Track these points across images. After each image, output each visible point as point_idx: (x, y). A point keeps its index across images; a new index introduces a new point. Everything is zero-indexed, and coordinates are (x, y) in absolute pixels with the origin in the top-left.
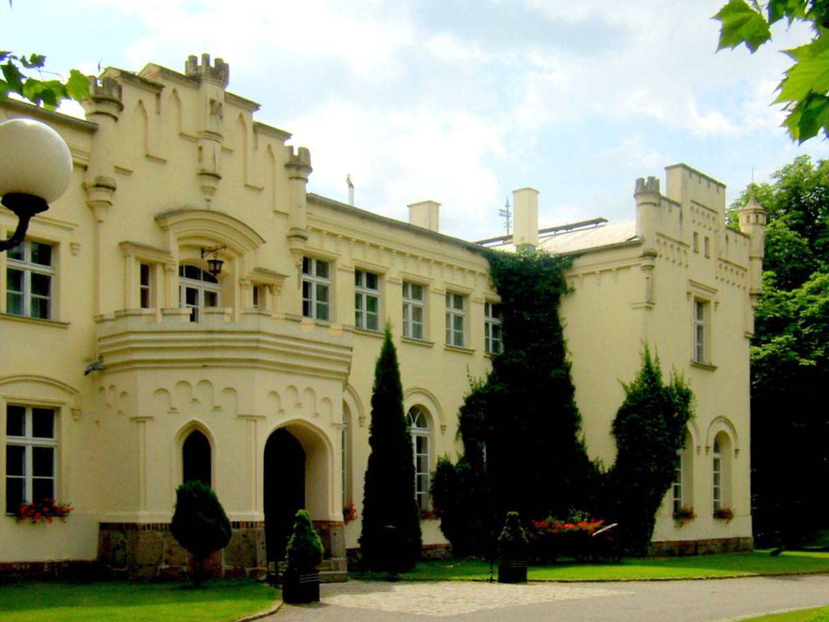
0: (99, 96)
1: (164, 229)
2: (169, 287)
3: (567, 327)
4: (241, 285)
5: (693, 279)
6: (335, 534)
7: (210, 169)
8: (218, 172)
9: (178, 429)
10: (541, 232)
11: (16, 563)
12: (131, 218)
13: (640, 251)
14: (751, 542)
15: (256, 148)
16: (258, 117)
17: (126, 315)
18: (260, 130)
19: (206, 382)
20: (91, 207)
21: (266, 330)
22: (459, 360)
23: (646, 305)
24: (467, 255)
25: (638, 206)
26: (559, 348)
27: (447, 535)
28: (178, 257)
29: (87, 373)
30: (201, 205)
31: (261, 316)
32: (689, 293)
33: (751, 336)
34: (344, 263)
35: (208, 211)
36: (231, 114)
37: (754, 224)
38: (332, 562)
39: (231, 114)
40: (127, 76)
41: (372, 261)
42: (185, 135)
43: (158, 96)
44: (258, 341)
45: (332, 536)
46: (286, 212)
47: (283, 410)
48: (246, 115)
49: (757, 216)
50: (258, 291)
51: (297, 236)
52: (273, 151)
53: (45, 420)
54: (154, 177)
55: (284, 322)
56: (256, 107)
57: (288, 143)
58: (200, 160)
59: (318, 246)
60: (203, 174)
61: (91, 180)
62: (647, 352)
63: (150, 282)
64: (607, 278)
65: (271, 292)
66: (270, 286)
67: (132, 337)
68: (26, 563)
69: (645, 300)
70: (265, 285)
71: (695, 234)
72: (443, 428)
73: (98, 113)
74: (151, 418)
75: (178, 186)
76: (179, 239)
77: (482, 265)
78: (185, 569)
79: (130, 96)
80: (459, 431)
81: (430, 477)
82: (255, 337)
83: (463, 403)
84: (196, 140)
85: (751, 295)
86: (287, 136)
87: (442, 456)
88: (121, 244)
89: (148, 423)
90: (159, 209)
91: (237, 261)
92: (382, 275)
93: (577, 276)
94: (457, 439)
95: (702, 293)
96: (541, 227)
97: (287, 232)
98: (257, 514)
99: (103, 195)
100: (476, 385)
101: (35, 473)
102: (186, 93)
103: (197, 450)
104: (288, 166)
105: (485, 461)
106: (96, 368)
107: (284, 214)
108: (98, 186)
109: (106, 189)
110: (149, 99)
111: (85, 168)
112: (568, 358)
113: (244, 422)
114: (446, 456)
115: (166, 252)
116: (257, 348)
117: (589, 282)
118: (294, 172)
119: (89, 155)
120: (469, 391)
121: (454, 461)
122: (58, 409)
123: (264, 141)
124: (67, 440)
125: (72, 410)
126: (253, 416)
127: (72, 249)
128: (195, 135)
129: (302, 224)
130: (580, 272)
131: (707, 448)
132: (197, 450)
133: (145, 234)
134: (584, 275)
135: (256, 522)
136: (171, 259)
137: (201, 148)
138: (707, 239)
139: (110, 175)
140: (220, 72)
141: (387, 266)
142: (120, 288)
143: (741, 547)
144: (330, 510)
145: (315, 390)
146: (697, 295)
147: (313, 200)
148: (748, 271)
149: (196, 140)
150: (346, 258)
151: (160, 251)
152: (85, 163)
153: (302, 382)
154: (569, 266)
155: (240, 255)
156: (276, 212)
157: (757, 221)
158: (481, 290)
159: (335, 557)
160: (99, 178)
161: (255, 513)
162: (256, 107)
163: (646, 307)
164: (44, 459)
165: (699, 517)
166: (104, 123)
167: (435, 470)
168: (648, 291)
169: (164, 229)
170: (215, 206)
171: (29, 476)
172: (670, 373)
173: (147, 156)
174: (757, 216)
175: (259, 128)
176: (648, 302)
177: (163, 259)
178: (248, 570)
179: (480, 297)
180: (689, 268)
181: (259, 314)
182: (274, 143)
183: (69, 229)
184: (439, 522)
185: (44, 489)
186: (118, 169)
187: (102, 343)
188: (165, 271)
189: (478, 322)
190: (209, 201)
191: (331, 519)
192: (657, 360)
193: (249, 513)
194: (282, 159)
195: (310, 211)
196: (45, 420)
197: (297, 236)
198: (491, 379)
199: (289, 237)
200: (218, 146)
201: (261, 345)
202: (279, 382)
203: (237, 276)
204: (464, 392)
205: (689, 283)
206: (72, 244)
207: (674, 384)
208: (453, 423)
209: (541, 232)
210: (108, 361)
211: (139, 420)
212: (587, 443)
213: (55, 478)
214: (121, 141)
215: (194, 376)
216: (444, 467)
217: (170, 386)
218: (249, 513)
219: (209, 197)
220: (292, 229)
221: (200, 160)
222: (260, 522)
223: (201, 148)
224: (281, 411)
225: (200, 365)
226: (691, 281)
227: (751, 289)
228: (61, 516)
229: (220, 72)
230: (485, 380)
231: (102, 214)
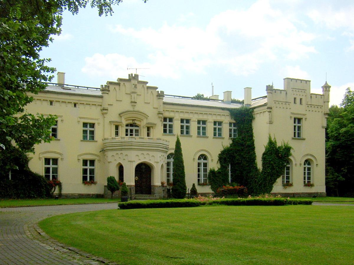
0: (103, 89)
1: (121, 117)
2: (122, 131)
3: (32, 159)
4: (143, 128)
5: (292, 112)
7: (133, 101)
9: (116, 164)
10: (252, 100)
11: (84, 194)
12: (113, 115)
13: (266, 107)
14: (325, 195)
15: (148, 93)
16: (148, 85)
18: (148, 88)
19: (121, 153)
20: (103, 114)
22: (218, 142)
23: (269, 123)
24: (221, 111)
25: (267, 93)
26: (251, 136)
27: (213, 190)
28: (125, 123)
29: (100, 152)
30: (132, 110)
32: (291, 117)
33: (326, 127)
34: (176, 119)
35: (134, 111)
36: (139, 86)
37: (325, 91)
38: (154, 195)
39: (139, 86)
40: (111, 83)
41: (186, 116)
43: (120, 85)
44: (132, 144)
45: (155, 189)
48: (144, 85)
49: (326, 88)
50: (148, 129)
51: (160, 113)
52: (153, 93)
53: (92, 162)
54: (119, 105)
55: (139, 139)
56: (147, 83)
57: (157, 90)
58: (131, 99)
59: (167, 115)
60: (132, 102)
61: (102, 108)
62: (270, 136)
63: (119, 129)
64: (262, 114)
65: (152, 128)
66: (152, 127)
67: (107, 144)
68: (86, 194)
69: (268, 121)
70: (151, 127)
71: (295, 99)
72: (212, 160)
73: (103, 93)
74: (111, 162)
75: (126, 106)
76: (125, 119)
77: (228, 113)
78: (117, 196)
79: (112, 87)
80: (218, 160)
81: (208, 174)
83: (220, 153)
84: (130, 94)
85: (324, 114)
86: (157, 88)
87: (212, 168)
88: (110, 122)
89: (111, 163)
90: (120, 112)
91: (142, 122)
92: (191, 120)
93: (255, 114)
94: (217, 163)
95: (296, 116)
96: (252, 99)
97: (157, 112)
98: (133, 183)
99: (105, 112)
100: (225, 147)
101: (49, 175)
102: (127, 84)
103: (121, 169)
104: (157, 96)
106: (103, 151)
108: (103, 109)
110: (117, 87)
111: (101, 105)
112: (254, 138)
113: (129, 162)
114: (213, 168)
115: (121, 122)
117: (258, 115)
118: (159, 97)
119: (102, 103)
120: (223, 149)
121: (216, 169)
122: (95, 160)
123: (150, 91)
124: (97, 167)
125: (98, 160)
127: (98, 124)
128: (130, 93)
129: (161, 110)
130: (256, 113)
131: (301, 164)
132: (121, 169)
133: (116, 118)
134: (257, 114)
137: (131, 96)
138: (301, 99)
139: (106, 106)
140: (136, 76)
141: (192, 117)
142: (110, 132)
143: (319, 196)
144: (154, 183)
145: (150, 154)
146: (294, 117)
147: (165, 103)
148: (323, 107)
149: (130, 94)
150: (177, 117)
151: (120, 122)
152: (101, 104)
153: (145, 152)
154: (253, 111)
155: (143, 120)
156: (154, 108)
157: (326, 90)
158: (227, 120)
160: (103, 108)
161: (132, 183)
162: (147, 83)
163: (269, 123)
164: (92, 172)
165: (294, 186)
166: (105, 96)
167: (209, 172)
168: (269, 118)
169: (121, 117)
171: (88, 175)
172: (282, 142)
173: (117, 100)
174: (326, 88)
175: (149, 88)
176: (270, 122)
177: (120, 124)
179: (227, 122)
180: (287, 109)
182: (153, 91)
184: (210, 186)
185: (92, 178)
186: (109, 105)
187: (105, 145)
188: (122, 127)
189: (226, 129)
190: (134, 108)
191: (155, 185)
192: (275, 138)
194: (155, 94)
195: (164, 106)
196: (92, 162)
197: (160, 113)
198: (231, 145)
199: (158, 114)
200: (136, 95)
202: (139, 153)
203: (142, 126)
204: (221, 150)
205: (291, 114)
206: (98, 123)
207: (283, 145)
208: (216, 158)
209: (252, 100)
210: (105, 149)
211: (109, 162)
212: (257, 163)
214: (109, 99)
215: (119, 152)
217: (115, 155)
219: (134, 107)
220: (158, 112)
221: (131, 99)
222: (133, 185)
223: (131, 96)
225: (120, 150)
226: (291, 113)
227: (324, 112)
228: (95, 184)
229: (136, 76)
230: (229, 146)
231: (105, 116)
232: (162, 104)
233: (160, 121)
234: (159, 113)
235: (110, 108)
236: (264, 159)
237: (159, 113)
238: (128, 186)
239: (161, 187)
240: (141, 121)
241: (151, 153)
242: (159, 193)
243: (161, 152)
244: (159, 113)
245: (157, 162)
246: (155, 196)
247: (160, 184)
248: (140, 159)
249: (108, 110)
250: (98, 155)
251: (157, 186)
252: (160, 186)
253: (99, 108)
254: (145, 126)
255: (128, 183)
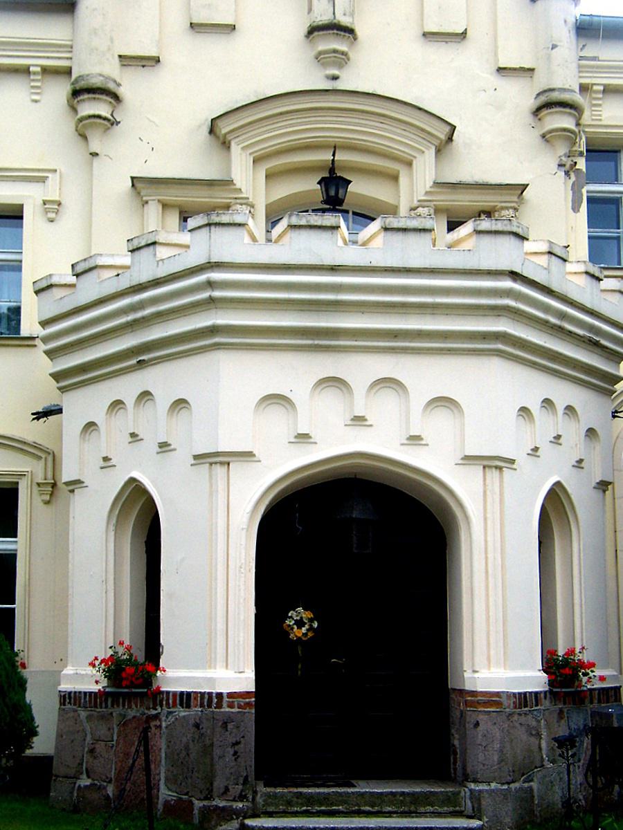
1: (226, 145)
6: (477, 724)
8: (345, 21)
17: (50, 286)
21: (226, 258)
31: (213, 228)
38: (465, 792)
42: (505, 69)
46: (526, 66)
47: (418, 438)
82: (202, 278)
97: (530, 103)
99: (101, 108)
105: (598, 758)
107: (522, 69)
109: (91, 96)
115: (227, 183)
116: (211, 301)
126: (217, 454)
135: (220, 695)
136: (235, 187)
139: (95, 65)
151: (210, 183)
153: (361, 369)
159: (475, 781)
170: (350, 80)
178: (198, 804)
181: (209, 225)
183: (37, 178)
186: (126, 61)
193: (209, 673)
199: (537, 111)
201: (217, 294)
202: (294, 373)
213: (18, 606)
215: (127, 387)
216: (166, 803)
218: (209, 673)
219: (336, 72)
224: (303, 438)
232: (566, 37)
233: (554, 166)
234: (543, 99)
235: (131, 85)
236: (513, 669)
237: (548, 104)
238: (185, 699)
239: (546, 703)
240: (395, 178)
241: (426, 376)
242: (525, 770)
243: (533, 365)
244: (548, 104)
245: (495, 464)
246: (476, 797)
247: (533, 678)
248: (305, 436)
249: (116, 97)
250: (35, 446)
251: (492, 699)
252: (524, 700)
253: (58, 92)
254: (422, 204)
255: (183, 673)
